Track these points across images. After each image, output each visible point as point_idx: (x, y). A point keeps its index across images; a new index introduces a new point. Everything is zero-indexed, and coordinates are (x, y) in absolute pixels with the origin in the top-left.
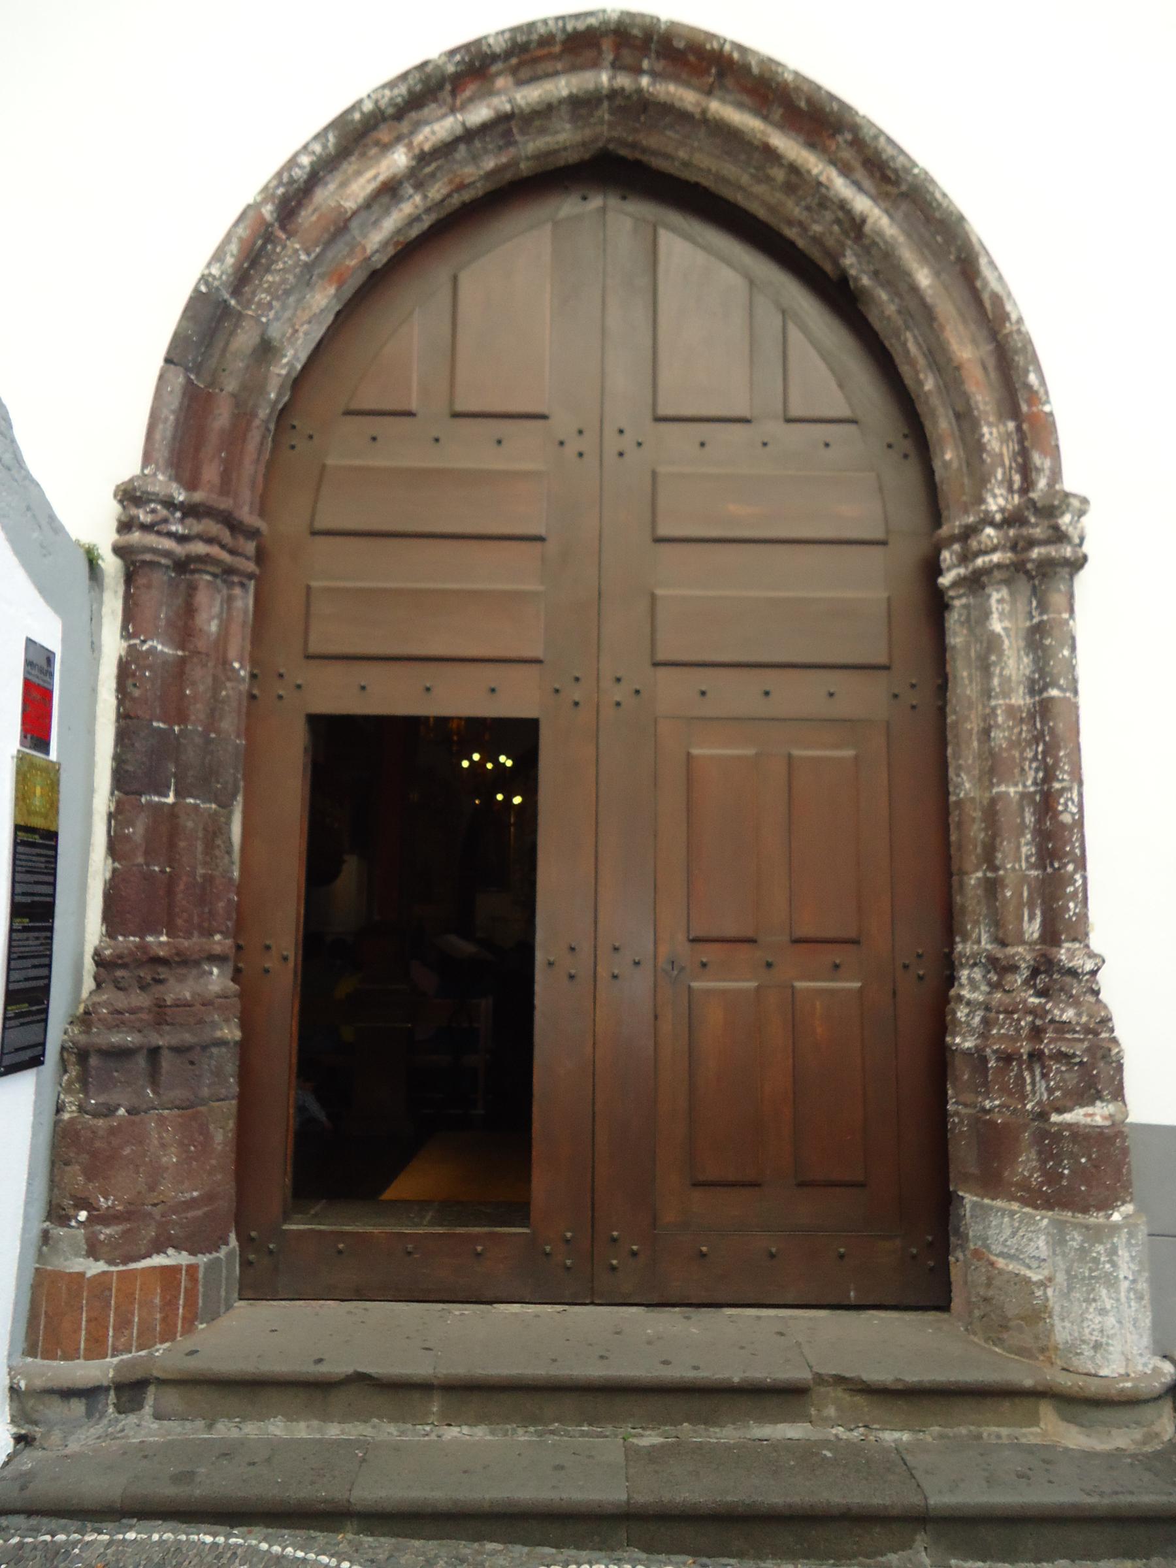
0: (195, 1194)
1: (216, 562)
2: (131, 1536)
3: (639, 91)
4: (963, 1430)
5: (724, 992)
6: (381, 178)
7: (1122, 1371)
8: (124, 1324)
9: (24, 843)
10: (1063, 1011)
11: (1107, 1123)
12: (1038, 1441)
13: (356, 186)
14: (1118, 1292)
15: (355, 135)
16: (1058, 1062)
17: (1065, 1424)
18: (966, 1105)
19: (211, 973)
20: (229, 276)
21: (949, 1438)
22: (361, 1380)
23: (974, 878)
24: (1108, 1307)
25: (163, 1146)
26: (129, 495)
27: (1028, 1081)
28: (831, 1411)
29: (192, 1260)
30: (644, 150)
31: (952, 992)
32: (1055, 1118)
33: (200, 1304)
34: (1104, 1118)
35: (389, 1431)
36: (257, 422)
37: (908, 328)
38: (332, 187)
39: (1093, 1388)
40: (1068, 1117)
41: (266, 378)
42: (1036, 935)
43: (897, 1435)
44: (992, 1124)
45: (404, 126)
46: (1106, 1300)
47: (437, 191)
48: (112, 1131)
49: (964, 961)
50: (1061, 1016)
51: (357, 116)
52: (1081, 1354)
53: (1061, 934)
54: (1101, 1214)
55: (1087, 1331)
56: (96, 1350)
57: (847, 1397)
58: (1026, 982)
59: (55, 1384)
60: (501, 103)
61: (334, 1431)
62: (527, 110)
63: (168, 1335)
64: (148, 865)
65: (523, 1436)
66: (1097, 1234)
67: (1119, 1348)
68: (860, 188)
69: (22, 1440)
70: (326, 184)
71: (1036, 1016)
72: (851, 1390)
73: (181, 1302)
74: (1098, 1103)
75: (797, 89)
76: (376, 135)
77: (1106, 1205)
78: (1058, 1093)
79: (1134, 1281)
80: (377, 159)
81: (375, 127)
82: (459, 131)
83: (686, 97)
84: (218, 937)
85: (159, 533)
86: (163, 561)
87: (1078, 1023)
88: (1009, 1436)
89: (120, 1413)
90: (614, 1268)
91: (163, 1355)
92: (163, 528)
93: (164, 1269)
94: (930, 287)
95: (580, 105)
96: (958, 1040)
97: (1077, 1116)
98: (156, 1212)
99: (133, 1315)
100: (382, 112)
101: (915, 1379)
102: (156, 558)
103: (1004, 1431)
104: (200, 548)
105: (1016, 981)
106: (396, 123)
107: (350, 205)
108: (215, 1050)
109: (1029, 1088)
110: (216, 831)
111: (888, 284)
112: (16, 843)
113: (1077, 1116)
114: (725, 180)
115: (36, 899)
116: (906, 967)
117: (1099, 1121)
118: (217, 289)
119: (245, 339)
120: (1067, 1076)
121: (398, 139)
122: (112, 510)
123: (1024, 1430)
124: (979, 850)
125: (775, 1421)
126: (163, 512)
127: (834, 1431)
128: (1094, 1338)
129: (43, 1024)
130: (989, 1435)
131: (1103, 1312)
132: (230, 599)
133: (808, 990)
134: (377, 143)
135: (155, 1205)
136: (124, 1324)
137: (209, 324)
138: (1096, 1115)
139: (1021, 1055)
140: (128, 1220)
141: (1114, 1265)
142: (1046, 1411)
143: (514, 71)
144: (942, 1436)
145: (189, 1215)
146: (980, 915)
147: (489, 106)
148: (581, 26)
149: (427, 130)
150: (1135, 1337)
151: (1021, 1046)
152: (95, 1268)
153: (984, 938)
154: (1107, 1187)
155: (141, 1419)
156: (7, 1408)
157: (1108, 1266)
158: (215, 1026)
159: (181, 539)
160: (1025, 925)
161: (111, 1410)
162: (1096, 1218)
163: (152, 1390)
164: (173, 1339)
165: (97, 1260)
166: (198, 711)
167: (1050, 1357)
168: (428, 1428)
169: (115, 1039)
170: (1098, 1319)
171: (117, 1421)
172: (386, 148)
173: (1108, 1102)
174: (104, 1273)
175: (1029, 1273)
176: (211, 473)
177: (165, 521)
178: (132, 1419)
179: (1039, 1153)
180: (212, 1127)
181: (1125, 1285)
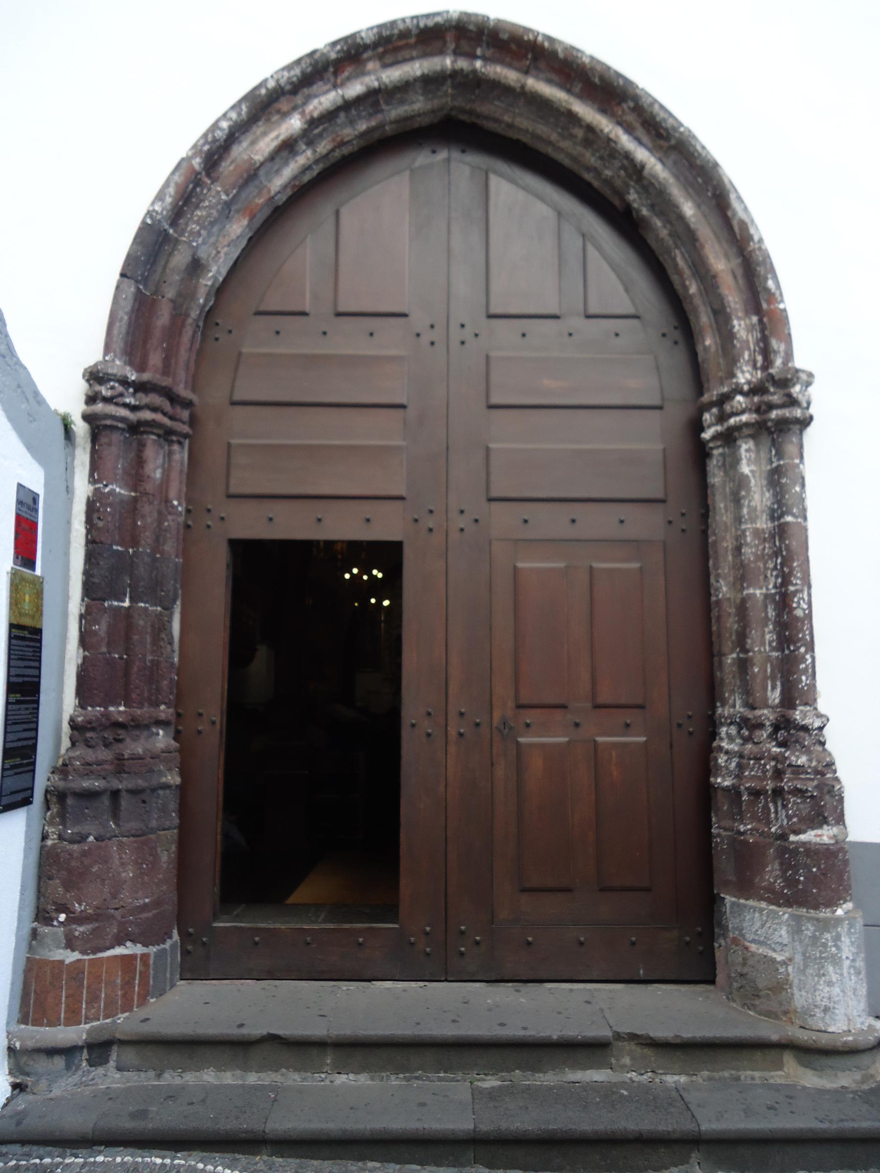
0: (147, 900)
2: (100, 1159)
3: (474, 71)
4: (726, 1074)
5: (543, 745)
6: (282, 137)
7: (845, 1028)
8: (93, 999)
9: (17, 638)
10: (798, 757)
11: (832, 842)
12: (783, 1081)
13: (263, 144)
14: (841, 968)
15: (262, 105)
16: (795, 795)
17: (802, 1069)
18: (725, 829)
19: (158, 734)
21: (715, 1080)
23: (730, 659)
24: (834, 980)
27: (773, 810)
28: (627, 1060)
29: (145, 950)
30: (479, 116)
31: (715, 744)
32: (793, 838)
34: (830, 838)
35: (292, 1078)
38: (245, 144)
39: (824, 1041)
40: (803, 837)
42: (777, 701)
43: (676, 1078)
45: (299, 99)
46: (833, 975)
47: (323, 147)
48: (84, 854)
49: (723, 720)
51: (263, 91)
52: (814, 1015)
54: (828, 910)
55: (818, 998)
56: (73, 1018)
57: (638, 1050)
61: (252, 1078)
62: (390, 86)
63: (127, 1007)
65: (395, 1081)
66: (826, 925)
69: (17, 1087)
70: (240, 142)
73: (137, 982)
74: (825, 827)
75: (592, 69)
77: (832, 903)
78: (795, 820)
80: (278, 123)
82: (340, 101)
83: (510, 75)
84: (163, 707)
85: (117, 404)
87: (809, 767)
88: (760, 1078)
89: (91, 1066)
91: (124, 1022)
92: (120, 400)
93: (123, 957)
94: (694, 216)
96: (719, 780)
101: (690, 1035)
102: (115, 423)
103: (757, 1074)
104: (147, 415)
105: (762, 735)
107: (258, 158)
109: (773, 816)
110: (161, 627)
111: (661, 214)
114: (539, 138)
115: (26, 679)
116: (679, 725)
117: (826, 840)
119: (180, 259)
121: (294, 108)
123: (772, 1073)
124: (734, 637)
125: (584, 1068)
126: (120, 388)
127: (629, 1075)
131: (830, 984)
132: (170, 454)
136: (93, 999)
138: (823, 835)
142: (789, 1059)
143: (381, 57)
144: (710, 1079)
146: (735, 685)
147: (362, 84)
148: (430, 23)
151: (767, 784)
153: (738, 703)
155: (107, 1070)
156: (6, 1063)
157: (834, 949)
159: (133, 408)
160: (769, 693)
161: (84, 1064)
162: (824, 913)
165: (73, 950)
168: (323, 1076)
170: (827, 989)
172: (285, 115)
174: (79, 960)
175: (774, 955)
176: (155, 359)
177: (121, 395)
178: (100, 1070)
179: (781, 864)
180: (159, 850)
181: (847, 963)
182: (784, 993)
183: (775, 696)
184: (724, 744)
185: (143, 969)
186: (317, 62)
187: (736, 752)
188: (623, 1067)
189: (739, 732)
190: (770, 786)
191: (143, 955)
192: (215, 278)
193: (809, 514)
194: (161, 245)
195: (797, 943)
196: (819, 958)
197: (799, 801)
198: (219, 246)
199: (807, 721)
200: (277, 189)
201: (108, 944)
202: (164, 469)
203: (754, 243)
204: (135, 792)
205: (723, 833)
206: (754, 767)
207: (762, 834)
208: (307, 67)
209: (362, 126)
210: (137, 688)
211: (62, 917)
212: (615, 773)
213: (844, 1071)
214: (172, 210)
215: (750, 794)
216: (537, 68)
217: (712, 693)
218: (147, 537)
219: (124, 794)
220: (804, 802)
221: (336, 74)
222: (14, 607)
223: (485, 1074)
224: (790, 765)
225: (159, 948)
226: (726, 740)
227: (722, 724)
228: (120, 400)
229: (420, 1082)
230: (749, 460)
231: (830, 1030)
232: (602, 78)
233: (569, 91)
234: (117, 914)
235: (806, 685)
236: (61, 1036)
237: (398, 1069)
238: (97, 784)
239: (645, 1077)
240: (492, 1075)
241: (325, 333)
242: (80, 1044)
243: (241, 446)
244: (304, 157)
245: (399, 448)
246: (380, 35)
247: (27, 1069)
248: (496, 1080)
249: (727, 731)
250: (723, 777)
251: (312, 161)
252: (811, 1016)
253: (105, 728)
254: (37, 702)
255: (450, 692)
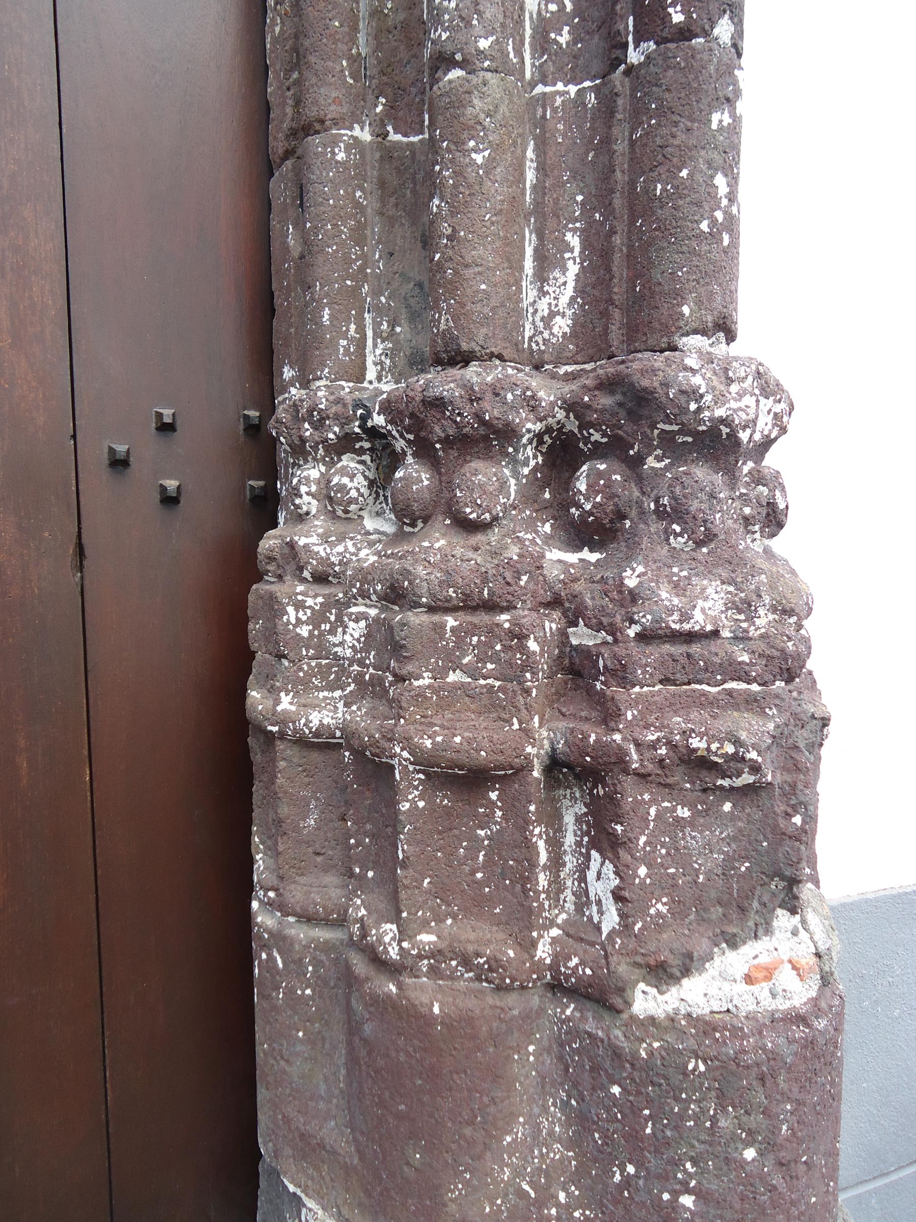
18: (308, 918)
23: (350, 140)
27: (543, 857)
31: (270, 542)
32: (646, 1001)
42: (562, 325)
44: (405, 1017)
49: (308, 430)
50: (685, 617)
53: (679, 296)
71: (574, 615)
87: (741, 638)
96: (286, 703)
105: (503, 485)
109: (543, 880)
116: (119, 463)
120: (693, 839)
124: (363, 45)
139: (523, 769)
146: (361, 276)
151: (527, 733)
153: (374, 354)
160: (529, 293)
179: (581, 1121)
183: (552, 304)
184: (309, 539)
187: (365, 575)
189: (379, 484)
190: (541, 737)
197: (684, 813)
205: (301, 933)
206: (460, 644)
207: (492, 974)
217: (268, 325)
226: (320, 524)
227: (300, 450)
247: (286, 550)
249: (325, 480)
250: (301, 687)
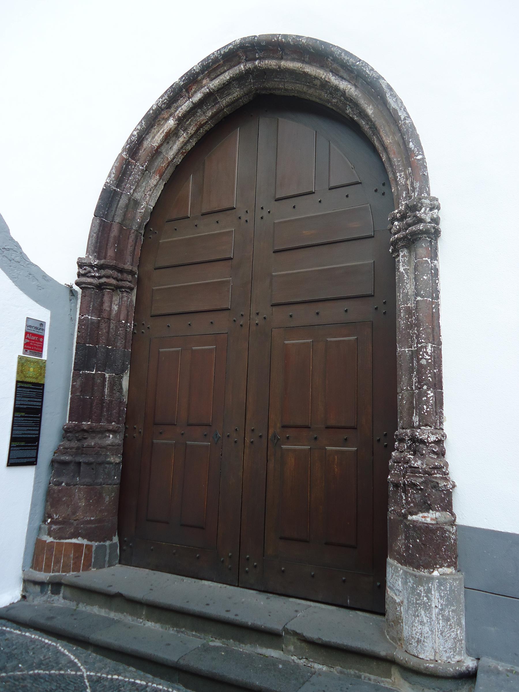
0: (92, 518)
1: (110, 285)
2: (27, 634)
3: (255, 67)
4: (352, 672)
5: (295, 450)
6: (165, 131)
7: (432, 658)
8: (57, 562)
9: (21, 387)
10: (416, 461)
11: (433, 522)
12: (389, 686)
13: (156, 138)
14: (430, 613)
15: (153, 119)
16: (412, 488)
17: (403, 681)
19: (109, 437)
20: (113, 181)
21: (345, 674)
22: (119, 595)
24: (425, 621)
25: (79, 499)
26: (81, 264)
28: (291, 648)
29: (89, 543)
30: (270, 89)
32: (410, 517)
33: (93, 560)
34: (432, 519)
35: (128, 619)
36: (133, 231)
37: (374, 135)
38: (149, 140)
39: (412, 662)
40: (414, 517)
41: (135, 214)
43: (320, 666)
45: (172, 110)
46: (424, 617)
47: (192, 130)
48: (60, 491)
51: (151, 112)
52: (411, 644)
54: (426, 571)
55: (414, 632)
56: (47, 570)
57: (299, 643)
58: (409, 448)
59: (32, 578)
60: (205, 90)
61: (113, 615)
62: (216, 89)
63: (76, 569)
64: (83, 396)
65: (172, 631)
66: (420, 581)
67: (431, 645)
68: (342, 78)
69: (24, 597)
70: (147, 139)
72: (300, 640)
73: (83, 558)
74: (431, 511)
75: (308, 45)
76: (162, 116)
77: (430, 566)
78: (412, 505)
79: (441, 610)
80: (163, 125)
81: (160, 113)
82: (191, 105)
83: (271, 63)
84: (113, 423)
85: (88, 277)
86: (91, 286)
88: (375, 680)
89: (52, 594)
90: (247, 572)
91: (70, 576)
92: (89, 275)
93: (75, 544)
94: (373, 113)
95: (239, 79)
97: (418, 517)
98: (75, 523)
99: (61, 559)
100: (161, 108)
101: (327, 640)
102: (86, 286)
103: (372, 677)
104: (103, 280)
106: (168, 110)
107: (156, 144)
108: (107, 466)
110: (116, 384)
111: (363, 118)
112: (17, 387)
113: (418, 517)
114: (298, 91)
115: (29, 406)
117: (429, 520)
118: (109, 186)
119: (123, 202)
120: (416, 496)
121: (171, 115)
122: (75, 269)
123: (383, 679)
125: (268, 647)
126: (88, 269)
127: (293, 658)
128: (417, 637)
129: (36, 451)
130: (365, 677)
131: (422, 623)
132: (122, 297)
133: (332, 451)
134: (163, 119)
135: (76, 520)
136: (57, 562)
137: (109, 199)
138: (428, 517)
140: (63, 524)
141: (429, 599)
142: (395, 672)
143: (208, 76)
144: (341, 672)
145: (88, 526)
147: (200, 93)
148: (226, 50)
149: (180, 109)
150: (442, 641)
152: (49, 539)
154: (430, 557)
155: (59, 598)
156: (22, 585)
157: (425, 599)
158: (107, 456)
159: (99, 277)
161: (49, 592)
162: (424, 573)
163: (63, 587)
164: (79, 571)
165: (50, 537)
166: (103, 339)
167: (401, 644)
168: (141, 620)
169: (62, 458)
170: (420, 627)
171: (51, 596)
172: (167, 119)
173: (437, 511)
174: (52, 542)
175: (396, 598)
176: (111, 253)
177: (90, 272)
178: (56, 597)
180: (104, 495)
181: (435, 611)
182: (399, 625)
185: (87, 553)
186: (174, 88)
188: (289, 651)
191: (87, 545)
192: (146, 208)
193: (441, 295)
194: (113, 198)
195: (405, 591)
196: (421, 605)
198: (148, 194)
199: (424, 437)
200: (172, 157)
201: (67, 536)
202: (119, 306)
203: (401, 121)
204: (89, 464)
208: (170, 93)
209: (209, 114)
210: (95, 413)
211: (49, 520)
212: (336, 470)
213: (430, 689)
214: (116, 180)
215: (394, 486)
216: (286, 54)
218: (103, 339)
219: (82, 464)
220: (417, 493)
221: (187, 91)
222: (20, 373)
223: (216, 639)
224: (410, 467)
225: (100, 544)
228: (89, 275)
229: (183, 635)
230: (404, 262)
231: (420, 656)
232: (313, 48)
233: (303, 62)
234: (75, 523)
235: (427, 411)
236: (38, 576)
237: (175, 625)
238: (67, 458)
239: (302, 661)
240: (219, 639)
241: (196, 226)
242: (46, 581)
243: (157, 290)
244: (183, 137)
245: (228, 282)
246: (202, 65)
248: (221, 643)
251: (187, 139)
252: (410, 644)
253: (78, 432)
254: (40, 417)
255: (247, 417)
